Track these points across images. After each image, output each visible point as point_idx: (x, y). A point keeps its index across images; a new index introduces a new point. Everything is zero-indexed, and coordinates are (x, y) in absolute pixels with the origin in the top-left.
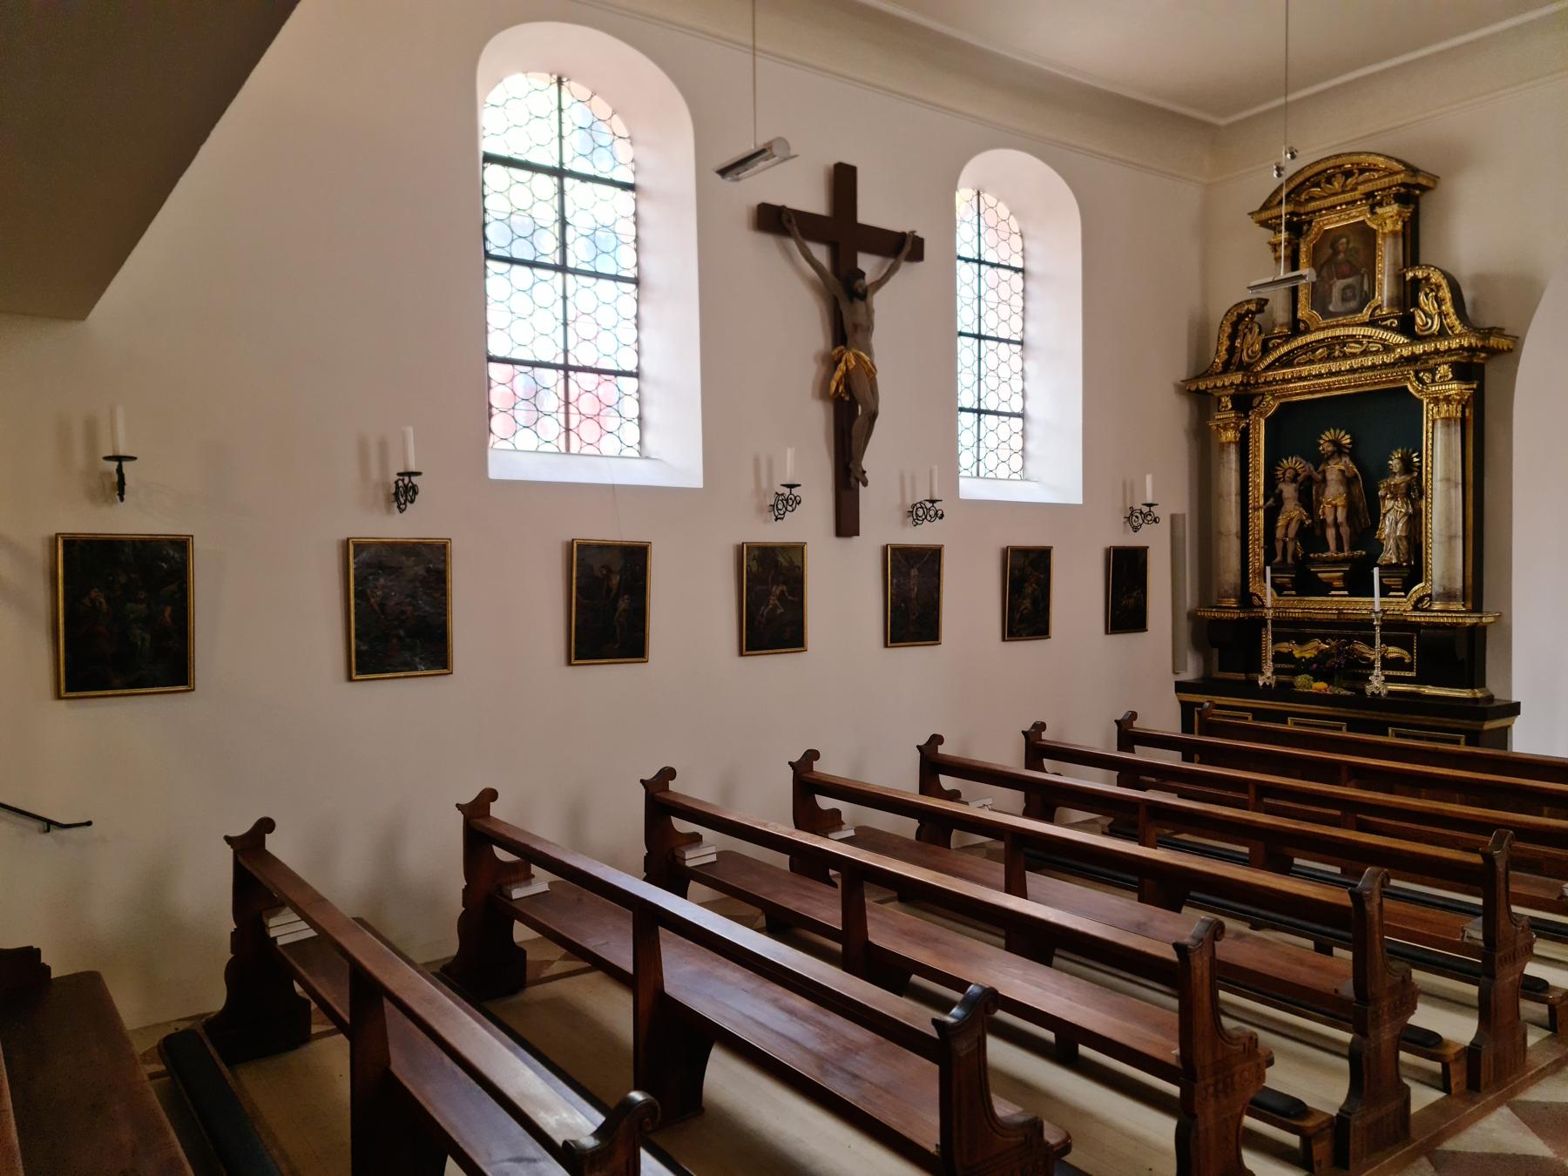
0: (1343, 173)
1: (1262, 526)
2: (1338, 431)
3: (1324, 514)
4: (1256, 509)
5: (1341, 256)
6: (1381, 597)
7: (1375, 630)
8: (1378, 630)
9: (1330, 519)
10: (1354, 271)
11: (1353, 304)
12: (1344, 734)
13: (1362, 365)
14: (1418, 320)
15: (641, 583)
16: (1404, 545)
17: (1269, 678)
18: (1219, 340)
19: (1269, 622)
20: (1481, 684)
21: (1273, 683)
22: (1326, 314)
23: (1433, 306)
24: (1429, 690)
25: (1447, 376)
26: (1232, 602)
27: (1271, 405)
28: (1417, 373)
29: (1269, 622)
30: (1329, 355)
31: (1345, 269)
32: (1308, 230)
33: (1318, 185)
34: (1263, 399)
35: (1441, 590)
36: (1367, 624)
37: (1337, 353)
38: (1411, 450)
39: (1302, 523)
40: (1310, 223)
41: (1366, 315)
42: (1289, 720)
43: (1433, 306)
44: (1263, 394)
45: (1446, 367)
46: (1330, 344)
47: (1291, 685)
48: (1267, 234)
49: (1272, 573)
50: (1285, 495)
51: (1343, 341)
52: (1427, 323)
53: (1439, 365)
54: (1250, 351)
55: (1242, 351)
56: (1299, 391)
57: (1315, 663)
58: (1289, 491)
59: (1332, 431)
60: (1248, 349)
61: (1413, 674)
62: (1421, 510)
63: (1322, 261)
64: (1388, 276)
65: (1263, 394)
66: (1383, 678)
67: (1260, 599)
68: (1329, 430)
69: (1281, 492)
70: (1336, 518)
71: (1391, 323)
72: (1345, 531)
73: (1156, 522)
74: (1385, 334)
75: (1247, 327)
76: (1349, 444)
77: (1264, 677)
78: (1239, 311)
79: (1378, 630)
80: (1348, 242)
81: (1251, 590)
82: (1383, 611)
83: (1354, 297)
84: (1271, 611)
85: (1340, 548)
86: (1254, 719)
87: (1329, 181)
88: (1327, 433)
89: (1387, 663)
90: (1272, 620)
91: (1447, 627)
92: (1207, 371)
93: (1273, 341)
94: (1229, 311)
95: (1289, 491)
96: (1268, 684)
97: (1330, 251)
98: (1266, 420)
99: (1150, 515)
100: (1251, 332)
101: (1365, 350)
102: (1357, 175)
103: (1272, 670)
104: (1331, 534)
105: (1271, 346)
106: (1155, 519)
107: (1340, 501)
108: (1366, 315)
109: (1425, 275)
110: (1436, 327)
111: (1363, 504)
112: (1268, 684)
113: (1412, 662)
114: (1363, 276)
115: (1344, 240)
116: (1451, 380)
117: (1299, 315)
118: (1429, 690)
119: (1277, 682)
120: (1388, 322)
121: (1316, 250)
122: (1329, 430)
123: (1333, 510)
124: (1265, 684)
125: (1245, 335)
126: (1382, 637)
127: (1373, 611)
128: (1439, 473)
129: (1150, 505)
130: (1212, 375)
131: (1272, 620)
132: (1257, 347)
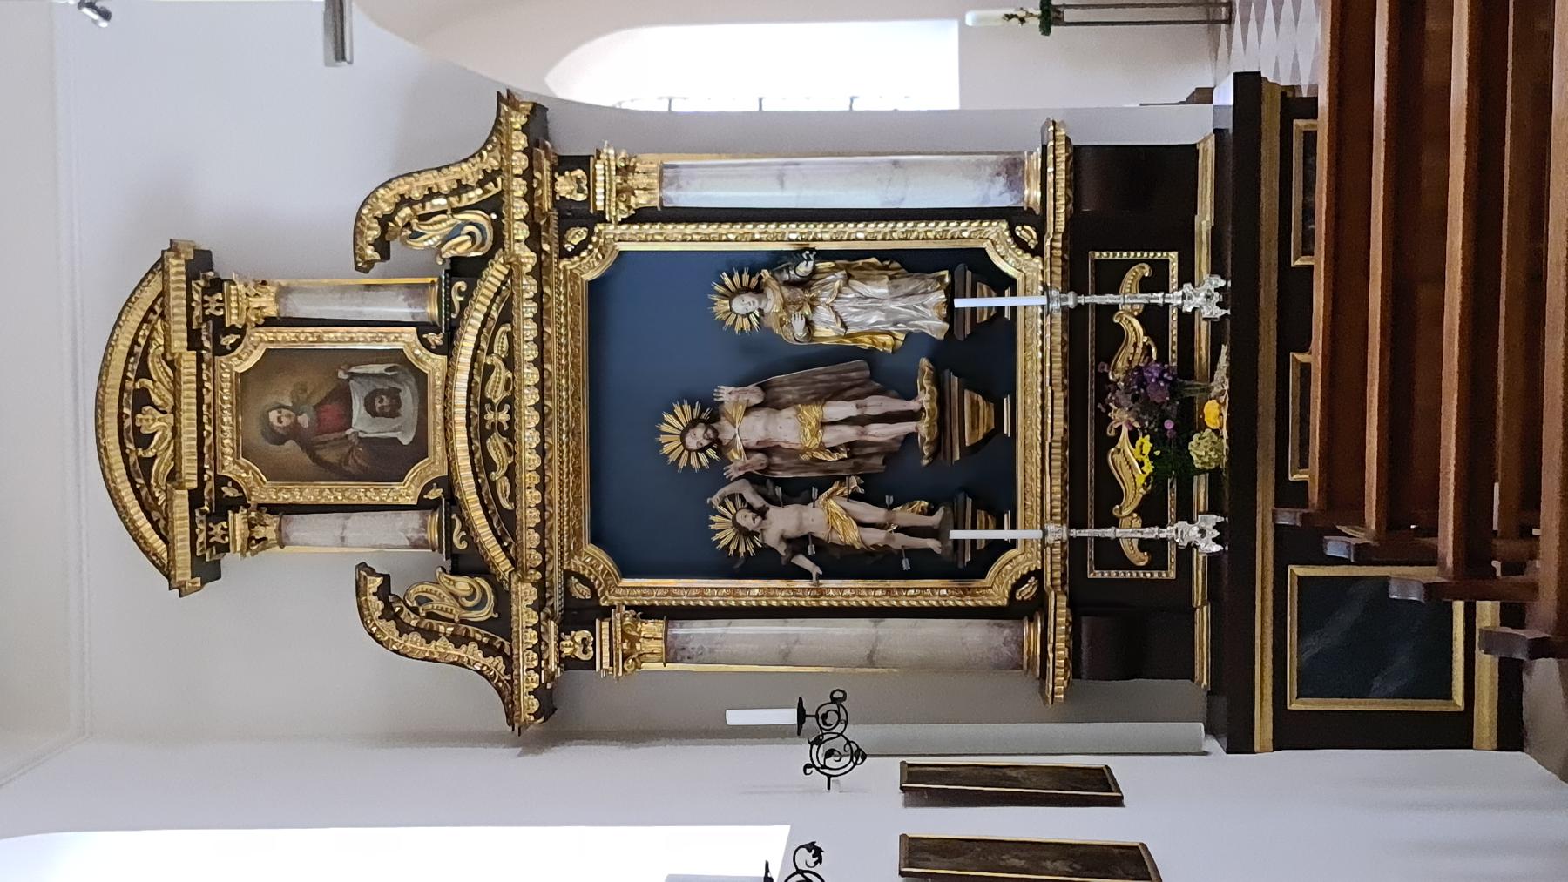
0: (137, 409)
1: (860, 583)
2: (665, 428)
3: (834, 449)
4: (822, 593)
5: (304, 420)
6: (1003, 528)
7: (1087, 304)
8: (1083, 300)
9: (850, 433)
10: (342, 396)
11: (408, 396)
12: (1314, 357)
13: (535, 341)
14: (461, 250)
15: (1120, 872)
16: (908, 284)
17: (1202, 532)
18: (435, 661)
19: (1075, 533)
20: (1191, 151)
21: (1215, 519)
22: (419, 450)
23: (440, 222)
24: (1204, 221)
25: (578, 181)
26: (1031, 633)
27: (594, 560)
28: (564, 254)
29: (1075, 533)
30: (503, 434)
31: (333, 408)
32: (236, 485)
33: (147, 464)
34: (577, 575)
35: (1002, 181)
36: (1074, 318)
37: (503, 417)
38: (718, 288)
39: (854, 496)
40: (221, 481)
41: (434, 364)
42: (1296, 477)
43: (440, 222)
44: (567, 574)
45: (560, 179)
46: (480, 432)
47: (1214, 476)
48: (229, 561)
49: (964, 528)
50: (792, 531)
51: (478, 399)
52: (470, 234)
53: (554, 193)
54: (469, 604)
55: (463, 621)
56: (570, 505)
57: (1162, 421)
58: (783, 521)
59: (663, 439)
60: (463, 607)
61: (1173, 256)
62: (826, 388)
63: (307, 459)
64: (363, 304)
65: (567, 574)
66: (1187, 287)
67: (1023, 580)
68: (666, 457)
69: (783, 538)
70: (848, 421)
71: (460, 293)
72: (877, 405)
73: (844, 698)
74: (481, 298)
75: (415, 610)
76: (693, 408)
77: (1202, 544)
78: (378, 614)
79: (1083, 300)
80: (280, 407)
81: (1005, 602)
82: (1046, 289)
83: (394, 395)
84: (1050, 527)
85: (913, 416)
86: (1305, 348)
87: (144, 440)
88: (666, 449)
89: (1156, 281)
90: (1071, 527)
91: (1075, 162)
92: (499, 690)
93: (456, 540)
94: (373, 635)
95: (783, 521)
96: (1217, 533)
97: (290, 444)
98: (624, 576)
99: (825, 716)
100: (429, 600)
101: (504, 360)
102: (148, 383)
103: (1182, 524)
104: (880, 433)
105: (464, 546)
106: (834, 700)
107: (813, 413)
108: (434, 364)
109: (376, 225)
110: (477, 217)
111: (821, 374)
112: (1217, 533)
113: (1147, 261)
114: (353, 375)
115: (273, 415)
116: (587, 171)
117: (414, 503)
118: (1204, 221)
119: (1213, 508)
120: (457, 299)
121: (277, 474)
122: (661, 445)
123: (828, 428)
124: (1216, 540)
125: (430, 615)
126: (1099, 291)
127: (1046, 312)
128: (770, 194)
129: (802, 715)
130: (511, 682)
131: (1071, 527)
132: (463, 584)
